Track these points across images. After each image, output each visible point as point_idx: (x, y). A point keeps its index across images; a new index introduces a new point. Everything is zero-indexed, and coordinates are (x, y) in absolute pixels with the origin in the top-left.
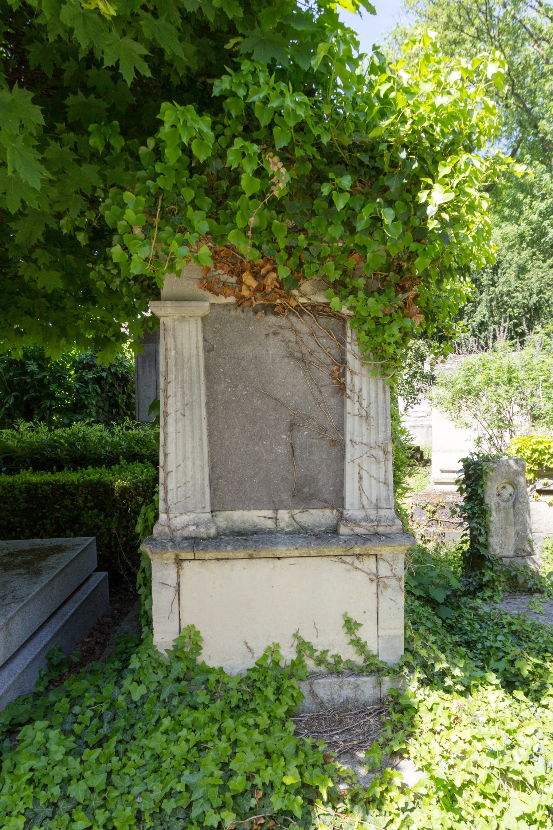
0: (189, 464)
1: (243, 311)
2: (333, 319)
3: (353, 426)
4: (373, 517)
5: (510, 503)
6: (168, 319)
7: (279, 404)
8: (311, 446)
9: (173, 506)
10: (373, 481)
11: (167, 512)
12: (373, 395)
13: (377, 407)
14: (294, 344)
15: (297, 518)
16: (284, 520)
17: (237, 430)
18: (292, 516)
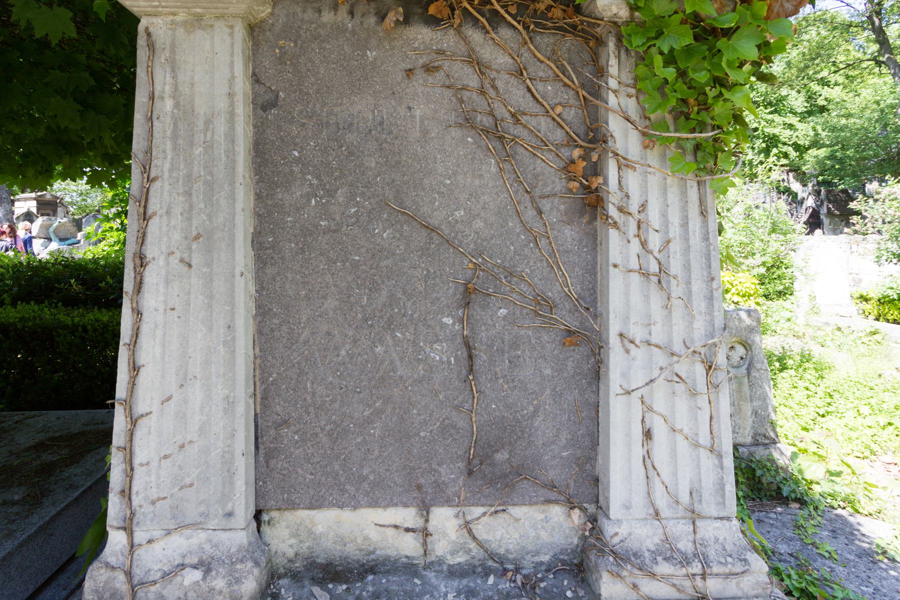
0: (196, 394)
1: (351, 13)
2: (569, 37)
3: (626, 302)
4: (685, 545)
5: (743, 370)
6: (158, 21)
7: (437, 239)
8: (515, 345)
9: (148, 509)
10: (682, 445)
11: (128, 528)
12: (675, 219)
13: (687, 250)
14: (475, 96)
15: (480, 530)
16: (445, 534)
17: (331, 303)
18: (467, 526)
